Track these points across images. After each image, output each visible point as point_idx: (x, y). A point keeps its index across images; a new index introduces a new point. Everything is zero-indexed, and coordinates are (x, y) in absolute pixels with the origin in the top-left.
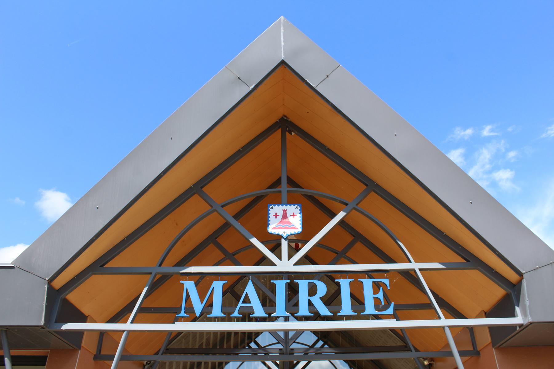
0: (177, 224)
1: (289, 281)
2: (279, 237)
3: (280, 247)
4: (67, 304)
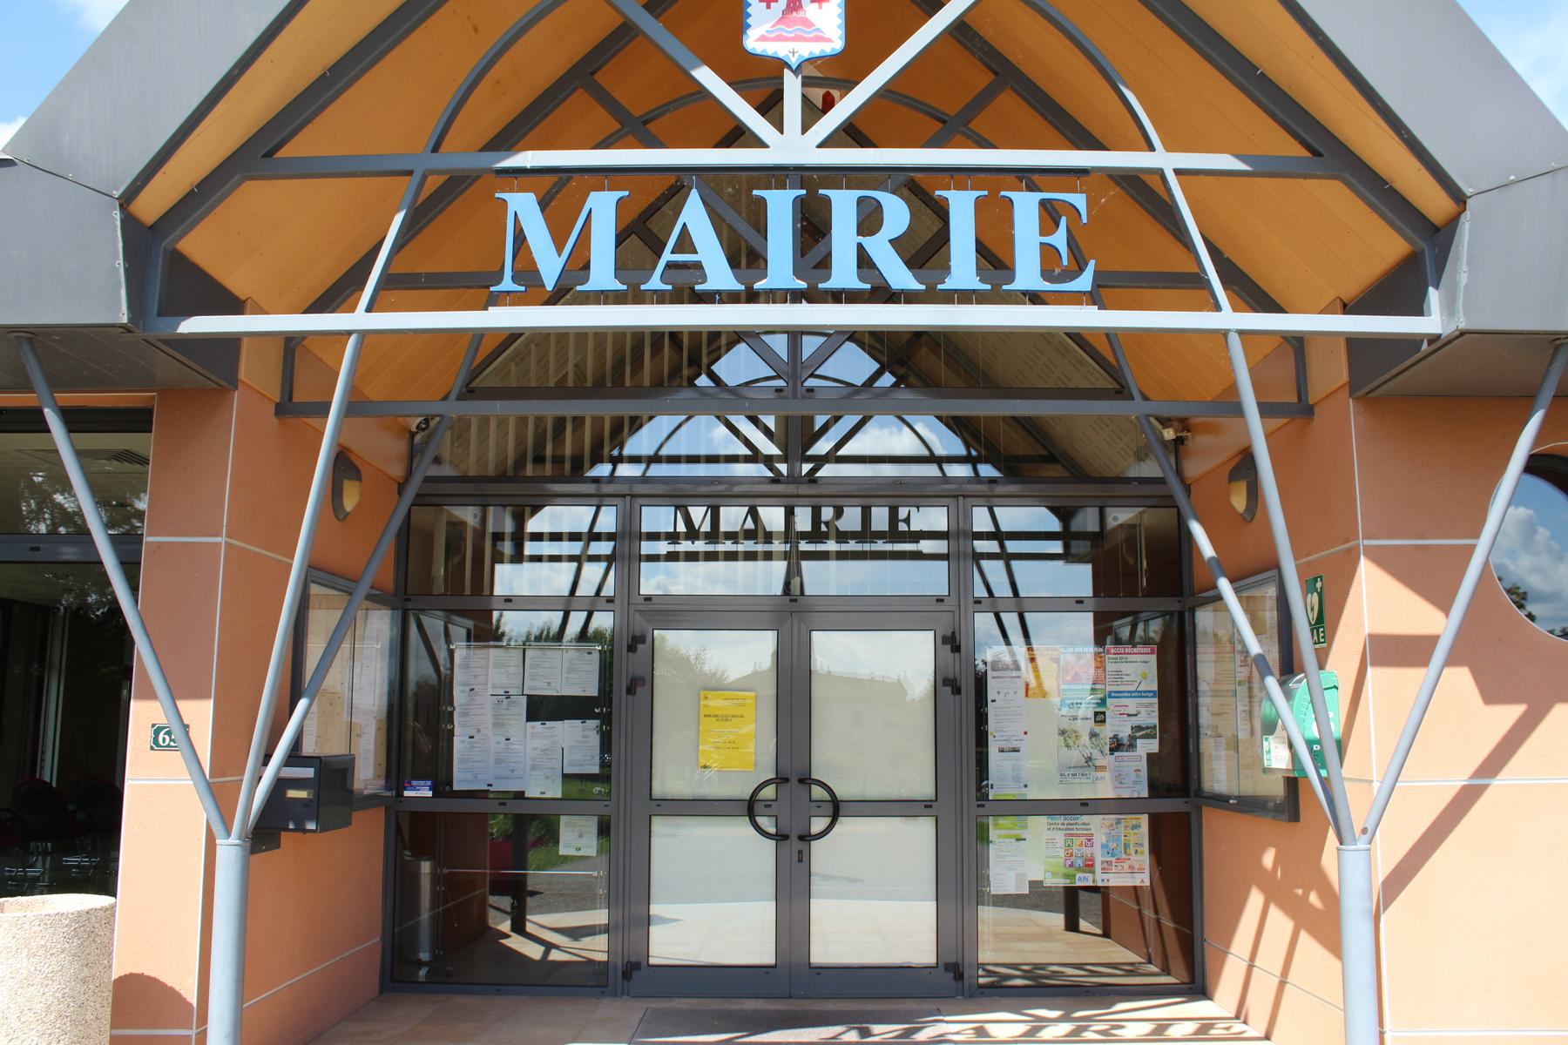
0: (476, 30)
1: (804, 192)
2: (777, 66)
3: (778, 105)
4: (181, 266)
